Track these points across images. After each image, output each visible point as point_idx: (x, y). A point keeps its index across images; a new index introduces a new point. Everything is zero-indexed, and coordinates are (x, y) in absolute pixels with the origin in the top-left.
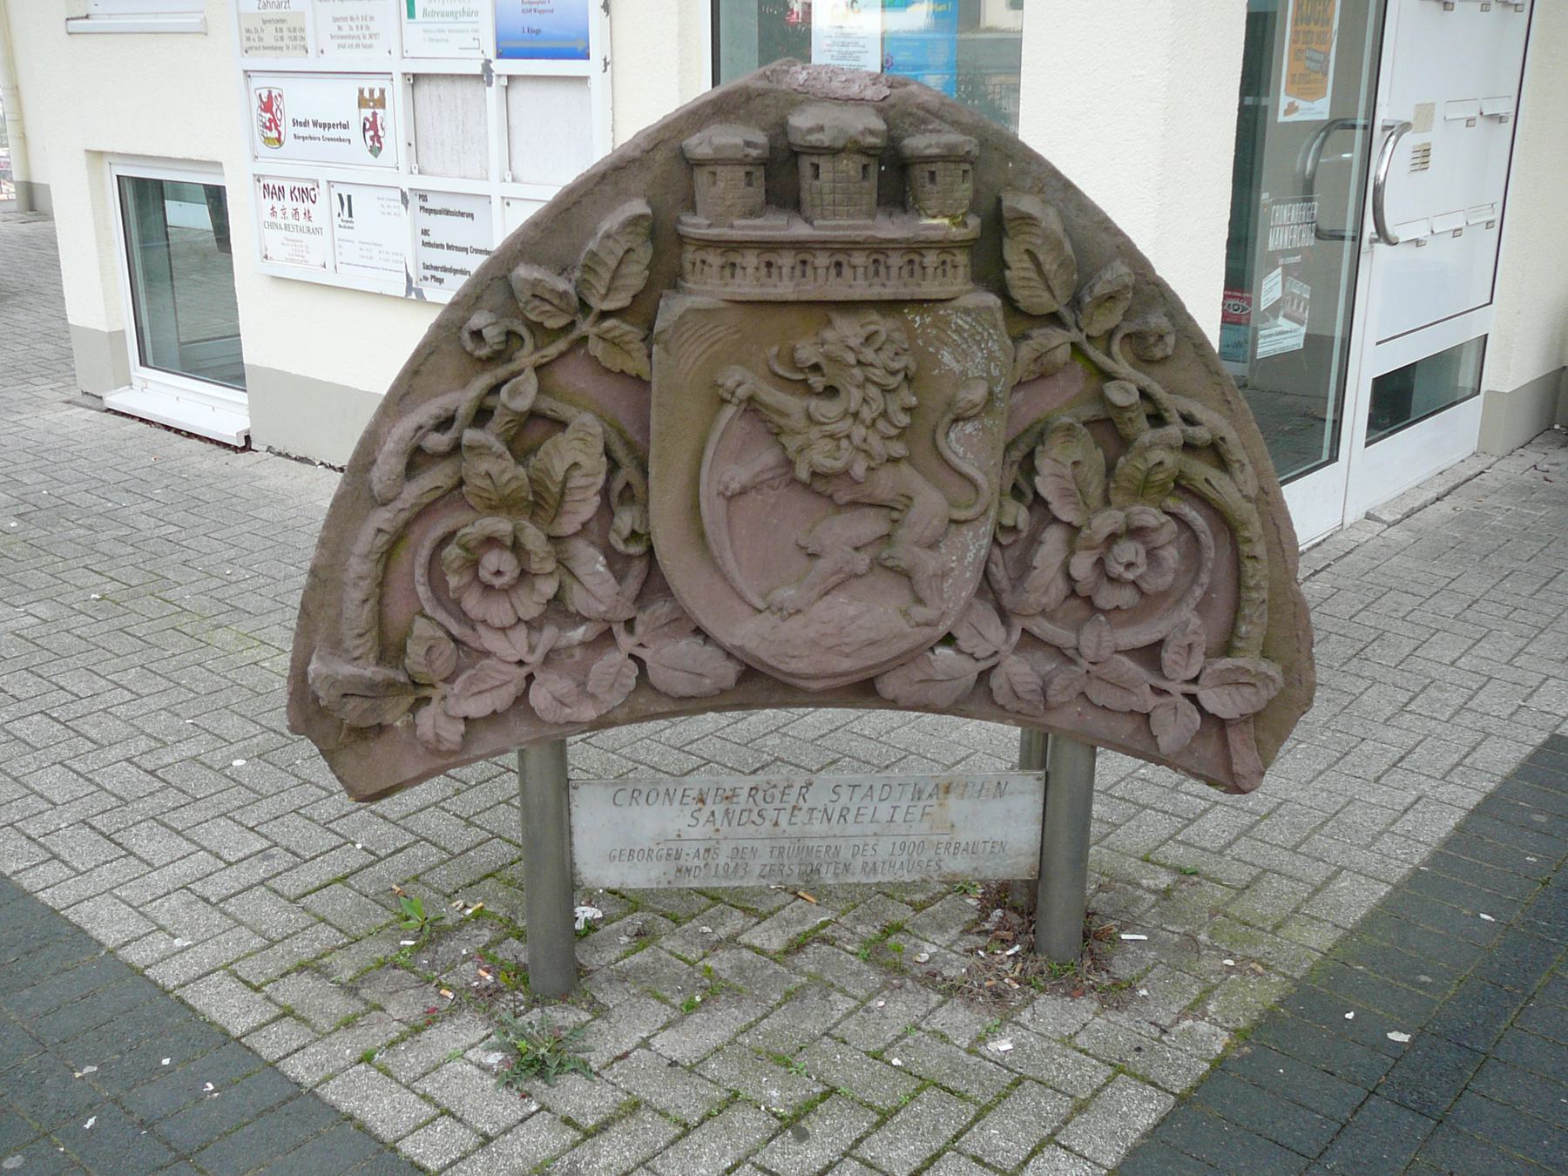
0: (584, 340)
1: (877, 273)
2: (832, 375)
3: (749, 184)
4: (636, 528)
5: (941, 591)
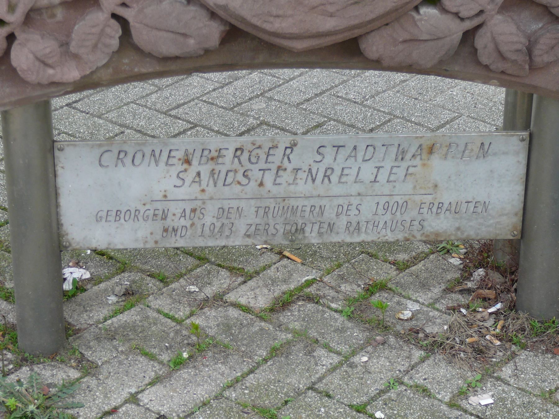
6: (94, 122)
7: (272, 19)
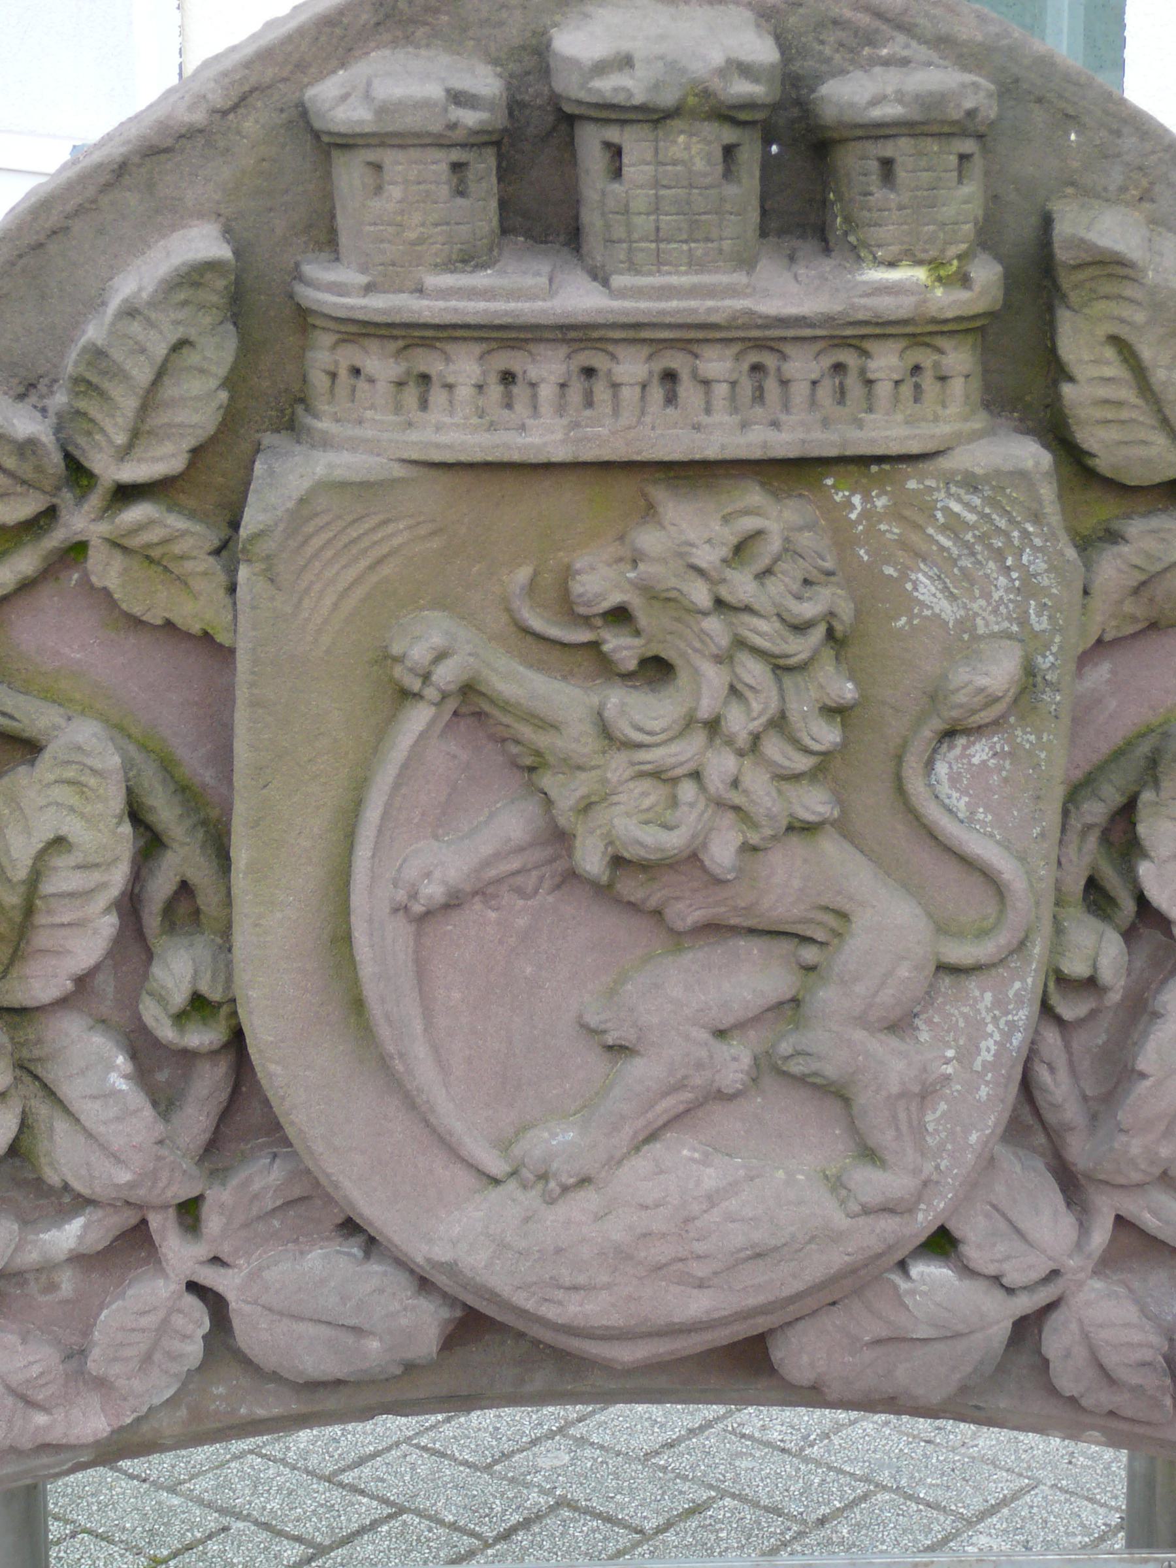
0: (78, 549)
1: (759, 396)
2: (656, 631)
3: (460, 192)
4: (204, 988)
5: (919, 1131)
6: (159, 1503)
7: (560, 1294)
